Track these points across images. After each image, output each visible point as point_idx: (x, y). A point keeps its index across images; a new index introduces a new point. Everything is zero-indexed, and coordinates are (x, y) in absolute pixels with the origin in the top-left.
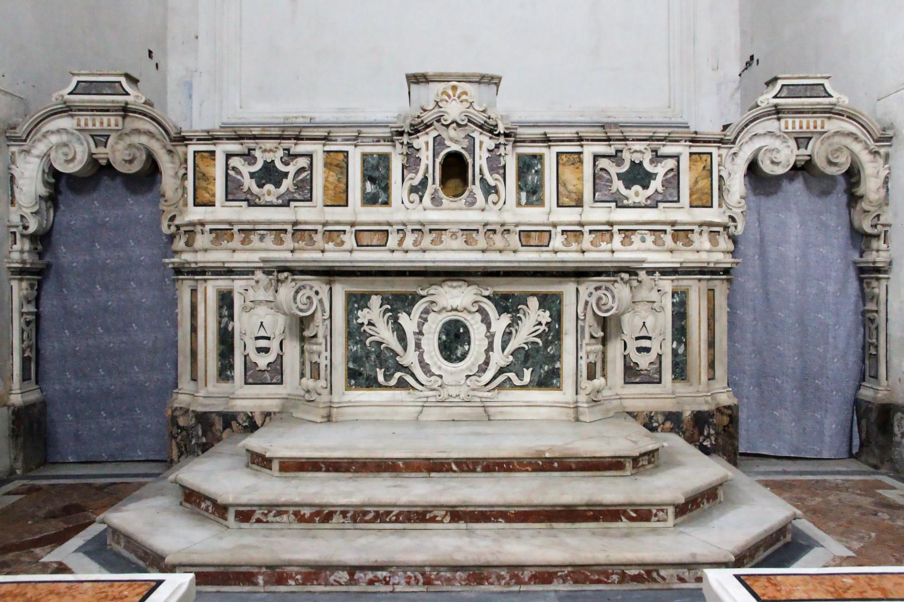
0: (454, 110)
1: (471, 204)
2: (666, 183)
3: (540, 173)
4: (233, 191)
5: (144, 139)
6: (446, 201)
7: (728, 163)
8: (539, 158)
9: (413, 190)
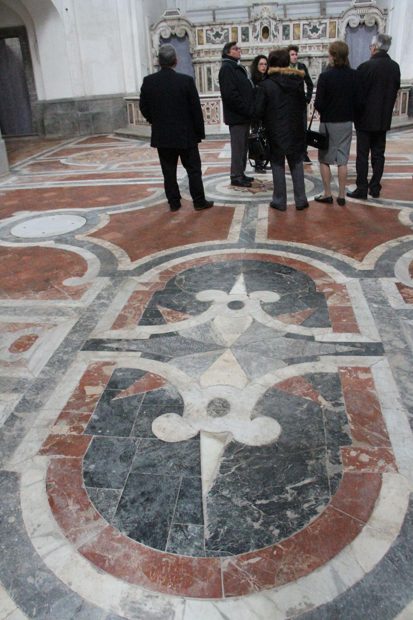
0: (265, 15)
1: (270, 41)
2: (323, 32)
3: (289, 30)
4: (209, 40)
5: (184, 27)
6: (264, 40)
7: (341, 24)
8: (288, 26)
9: (255, 37)
